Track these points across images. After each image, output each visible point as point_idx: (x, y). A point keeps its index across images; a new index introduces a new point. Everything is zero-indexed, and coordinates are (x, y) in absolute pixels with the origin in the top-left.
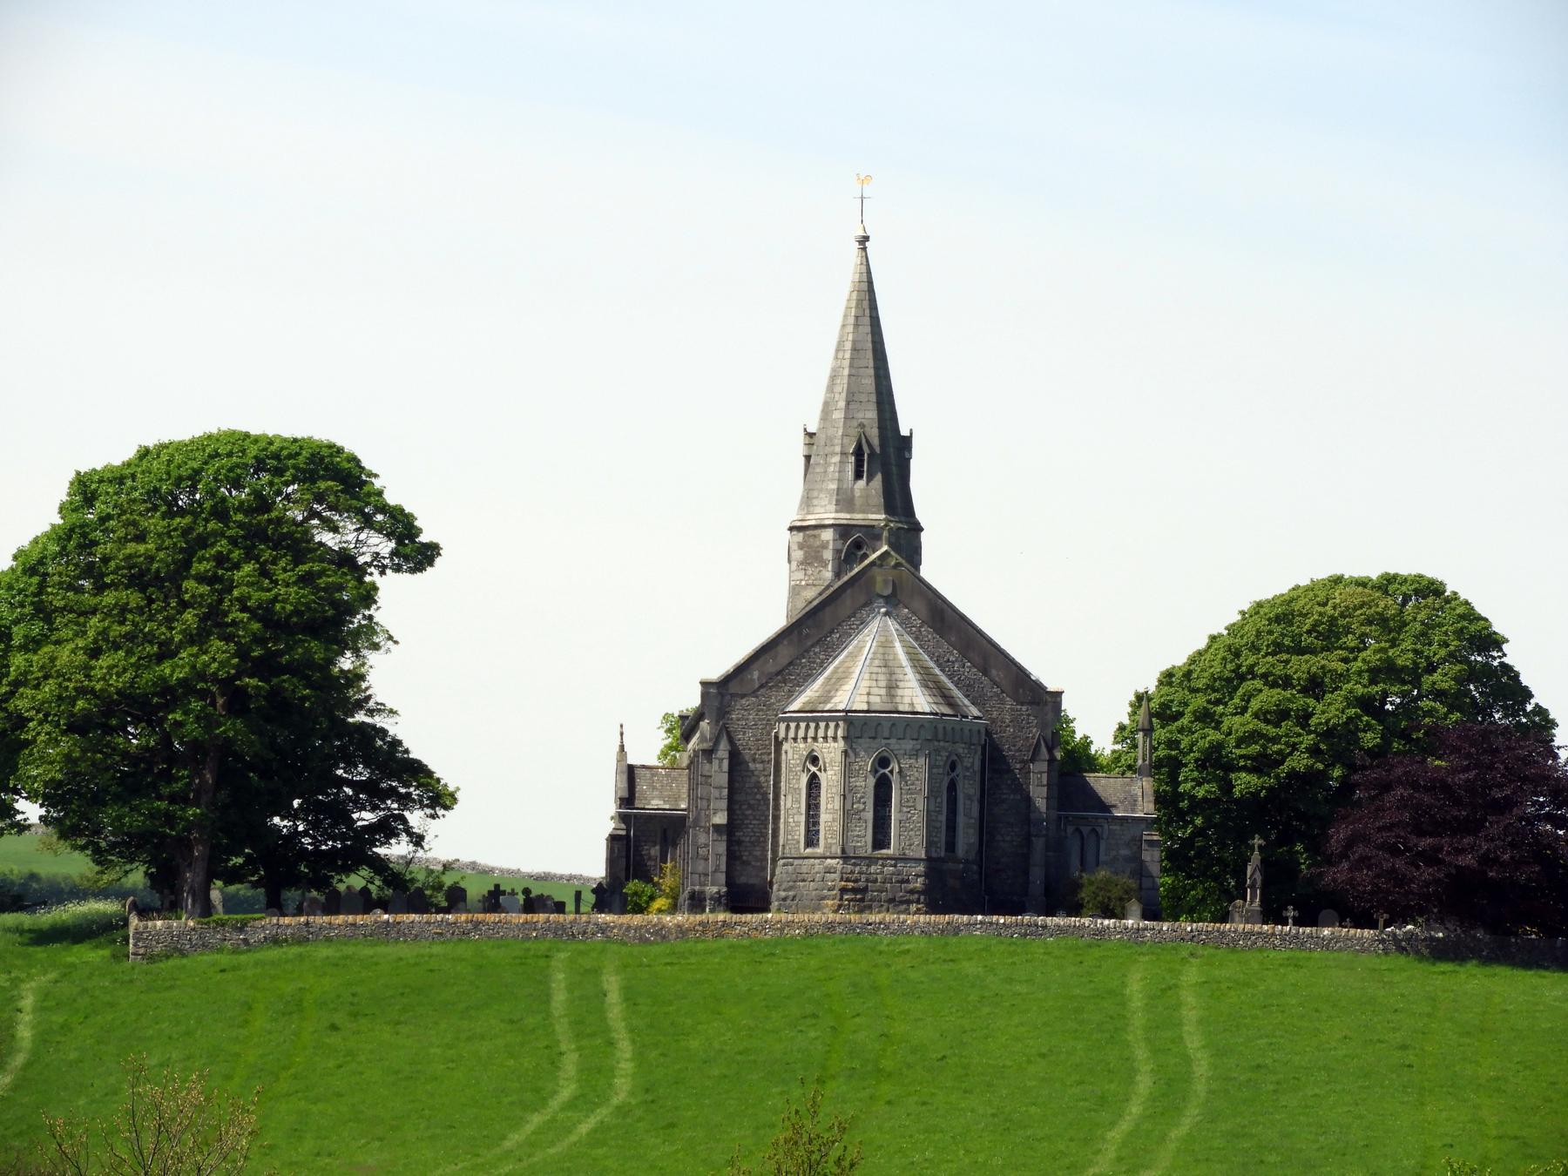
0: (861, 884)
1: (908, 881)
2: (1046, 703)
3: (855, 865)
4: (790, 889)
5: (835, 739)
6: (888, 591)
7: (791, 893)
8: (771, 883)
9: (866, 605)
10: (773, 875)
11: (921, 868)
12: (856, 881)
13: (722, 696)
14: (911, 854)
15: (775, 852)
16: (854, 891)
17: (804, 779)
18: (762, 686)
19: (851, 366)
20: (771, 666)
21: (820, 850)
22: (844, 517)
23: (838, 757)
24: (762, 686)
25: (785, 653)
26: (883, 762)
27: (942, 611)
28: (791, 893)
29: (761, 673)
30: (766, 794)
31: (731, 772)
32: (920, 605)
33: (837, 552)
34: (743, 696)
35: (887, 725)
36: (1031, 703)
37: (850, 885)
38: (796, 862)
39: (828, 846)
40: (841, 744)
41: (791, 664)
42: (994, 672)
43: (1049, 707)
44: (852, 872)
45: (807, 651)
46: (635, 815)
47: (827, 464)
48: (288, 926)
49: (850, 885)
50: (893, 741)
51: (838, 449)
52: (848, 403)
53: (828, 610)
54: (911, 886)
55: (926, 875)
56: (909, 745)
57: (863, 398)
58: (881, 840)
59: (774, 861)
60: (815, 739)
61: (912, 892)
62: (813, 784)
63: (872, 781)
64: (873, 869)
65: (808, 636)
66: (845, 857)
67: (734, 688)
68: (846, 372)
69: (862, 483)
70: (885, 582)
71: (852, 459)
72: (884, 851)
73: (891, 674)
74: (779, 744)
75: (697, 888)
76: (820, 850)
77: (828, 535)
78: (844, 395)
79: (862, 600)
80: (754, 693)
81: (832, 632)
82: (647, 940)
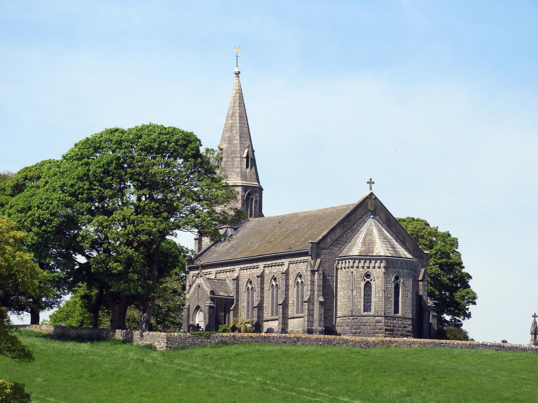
0: (391, 328)
1: (406, 327)
2: (424, 258)
3: (389, 320)
4: (358, 328)
5: (379, 268)
6: (372, 209)
7: (359, 331)
8: (335, 326)
9: (365, 214)
10: (335, 323)
11: (410, 322)
12: (390, 326)
13: (317, 248)
14: (406, 316)
15: (336, 315)
16: (390, 330)
17: (363, 284)
18: (331, 245)
19: (240, 123)
20: (334, 237)
21: (372, 313)
22: (245, 183)
23: (381, 275)
24: (331, 245)
25: (338, 232)
26: (397, 278)
27: (390, 219)
28: (359, 331)
29: (331, 240)
30: (333, 290)
31: (323, 280)
32: (382, 215)
33: (243, 196)
34: (325, 249)
35: (399, 262)
36: (419, 257)
37: (388, 328)
38: (359, 318)
39: (376, 311)
40: (383, 270)
41: (340, 236)
42: (407, 244)
43: (425, 260)
44: (388, 323)
45: (346, 232)
46: (216, 298)
47: (233, 161)
48: (227, 337)
49: (388, 328)
50: (400, 269)
51: (238, 155)
52: (240, 137)
53: (353, 216)
54: (408, 329)
55: (413, 325)
56: (406, 271)
57: (245, 136)
58: (396, 311)
59: (336, 318)
60: (368, 267)
61: (408, 331)
62: (368, 286)
63: (393, 285)
64: (395, 321)
65: (346, 226)
66: (386, 317)
67: (322, 245)
68: (238, 125)
69: (248, 170)
70: (372, 205)
71: (245, 160)
72: (397, 315)
73: (390, 242)
74: (337, 269)
75: (310, 327)
76: (372, 313)
77: (239, 189)
78: (238, 134)
79: (364, 212)
80: (328, 248)
81: (354, 224)
82: (363, 347)
